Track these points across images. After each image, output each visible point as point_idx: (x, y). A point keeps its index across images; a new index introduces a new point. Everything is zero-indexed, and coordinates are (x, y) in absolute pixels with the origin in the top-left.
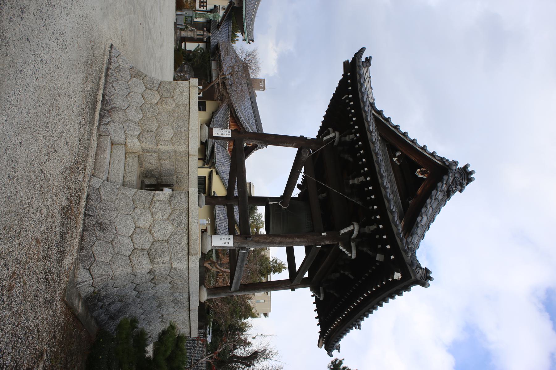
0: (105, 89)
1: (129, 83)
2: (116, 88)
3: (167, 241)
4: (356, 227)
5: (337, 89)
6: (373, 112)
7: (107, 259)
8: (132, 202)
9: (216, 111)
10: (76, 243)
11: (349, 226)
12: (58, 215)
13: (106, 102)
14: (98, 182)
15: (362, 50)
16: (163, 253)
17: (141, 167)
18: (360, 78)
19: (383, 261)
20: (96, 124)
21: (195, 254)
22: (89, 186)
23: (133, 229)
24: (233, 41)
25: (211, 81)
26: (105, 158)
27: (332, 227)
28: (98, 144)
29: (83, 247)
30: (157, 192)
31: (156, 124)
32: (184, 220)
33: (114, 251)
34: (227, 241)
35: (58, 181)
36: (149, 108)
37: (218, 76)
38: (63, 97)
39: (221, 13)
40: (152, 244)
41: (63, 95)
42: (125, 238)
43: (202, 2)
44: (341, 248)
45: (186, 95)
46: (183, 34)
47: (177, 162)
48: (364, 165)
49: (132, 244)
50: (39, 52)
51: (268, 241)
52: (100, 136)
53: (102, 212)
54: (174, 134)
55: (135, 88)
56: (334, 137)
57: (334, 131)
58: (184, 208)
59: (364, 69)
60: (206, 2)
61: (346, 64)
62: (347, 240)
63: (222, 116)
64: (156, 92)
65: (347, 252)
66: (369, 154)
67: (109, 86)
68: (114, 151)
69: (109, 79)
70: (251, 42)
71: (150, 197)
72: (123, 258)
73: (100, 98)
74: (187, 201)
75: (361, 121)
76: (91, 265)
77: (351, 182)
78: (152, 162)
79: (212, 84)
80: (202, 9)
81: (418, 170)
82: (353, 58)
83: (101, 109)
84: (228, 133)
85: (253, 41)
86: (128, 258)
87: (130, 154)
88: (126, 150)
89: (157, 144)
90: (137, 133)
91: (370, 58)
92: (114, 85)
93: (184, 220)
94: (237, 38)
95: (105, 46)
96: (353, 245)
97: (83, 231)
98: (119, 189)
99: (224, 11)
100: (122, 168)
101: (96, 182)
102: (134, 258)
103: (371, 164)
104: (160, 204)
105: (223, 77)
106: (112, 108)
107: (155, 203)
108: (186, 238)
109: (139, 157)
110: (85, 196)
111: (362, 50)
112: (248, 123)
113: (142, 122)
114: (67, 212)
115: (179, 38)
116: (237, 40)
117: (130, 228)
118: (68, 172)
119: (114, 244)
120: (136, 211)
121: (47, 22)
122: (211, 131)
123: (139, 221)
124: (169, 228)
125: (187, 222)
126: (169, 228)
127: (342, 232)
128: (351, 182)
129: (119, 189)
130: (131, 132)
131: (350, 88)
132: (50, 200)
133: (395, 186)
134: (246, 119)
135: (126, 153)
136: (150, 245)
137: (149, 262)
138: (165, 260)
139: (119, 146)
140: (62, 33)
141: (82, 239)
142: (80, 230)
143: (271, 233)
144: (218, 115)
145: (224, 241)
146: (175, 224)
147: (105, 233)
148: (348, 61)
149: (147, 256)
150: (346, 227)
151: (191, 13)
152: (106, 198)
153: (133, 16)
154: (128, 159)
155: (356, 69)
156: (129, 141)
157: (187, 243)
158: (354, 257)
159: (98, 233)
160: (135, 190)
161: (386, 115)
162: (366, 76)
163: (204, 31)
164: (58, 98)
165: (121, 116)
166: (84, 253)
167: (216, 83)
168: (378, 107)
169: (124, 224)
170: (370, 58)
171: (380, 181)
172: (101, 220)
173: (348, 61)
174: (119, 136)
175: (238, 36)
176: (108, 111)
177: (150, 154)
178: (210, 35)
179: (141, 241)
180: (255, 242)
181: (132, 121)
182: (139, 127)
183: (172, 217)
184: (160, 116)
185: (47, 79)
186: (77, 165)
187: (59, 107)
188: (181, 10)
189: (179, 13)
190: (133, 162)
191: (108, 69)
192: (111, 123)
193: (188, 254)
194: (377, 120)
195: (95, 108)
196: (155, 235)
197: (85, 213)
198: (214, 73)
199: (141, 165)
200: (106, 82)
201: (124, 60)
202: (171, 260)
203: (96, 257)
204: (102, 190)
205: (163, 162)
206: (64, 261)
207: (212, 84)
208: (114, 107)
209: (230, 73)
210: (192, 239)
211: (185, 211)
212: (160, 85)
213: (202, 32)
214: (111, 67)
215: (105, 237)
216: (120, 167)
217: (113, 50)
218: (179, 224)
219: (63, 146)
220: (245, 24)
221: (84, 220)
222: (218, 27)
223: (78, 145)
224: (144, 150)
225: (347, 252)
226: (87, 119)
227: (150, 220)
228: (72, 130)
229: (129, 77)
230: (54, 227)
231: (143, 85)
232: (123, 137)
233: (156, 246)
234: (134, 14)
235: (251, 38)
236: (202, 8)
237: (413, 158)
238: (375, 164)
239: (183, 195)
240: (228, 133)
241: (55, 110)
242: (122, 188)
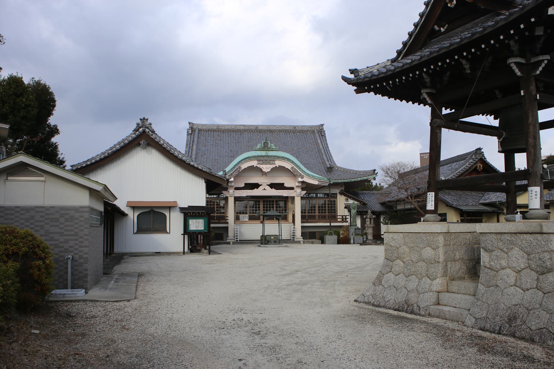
0: (390, 308)
1: (386, 286)
2: (390, 298)
3: (528, 255)
4: (511, 60)
5: (382, 96)
6: (400, 59)
7: (545, 316)
8: (491, 288)
9: (445, 203)
10: (522, 344)
11: (511, 67)
12: (483, 357)
13: (400, 308)
14: (470, 319)
15: (345, 79)
16: (540, 259)
17: (464, 278)
18: (367, 77)
19: (543, 27)
20: (418, 317)
21: (541, 227)
22: (472, 327)
23: (517, 288)
24: (382, 188)
25: (415, 209)
26: (449, 311)
27: (515, 85)
28: (437, 317)
29: (531, 338)
30: (481, 264)
31: (421, 264)
32: (507, 238)
33: (538, 308)
34: (534, 193)
35: (451, 353)
36: (408, 270)
37: (411, 203)
38: (379, 342)
39: (351, 201)
40: (532, 270)
41: (377, 342)
42: (525, 297)
43: (343, 220)
44: (538, 72)
45: (395, 236)
46: (370, 237)
47: (457, 244)
48: (497, 40)
49: (531, 290)
50: (335, 356)
51: (532, 151)
52: (430, 315)
53: (498, 317)
54: (429, 246)
55: (390, 281)
56: (427, 93)
57: (421, 94)
58: (496, 237)
59: (361, 74)
60: (342, 216)
61: (357, 92)
62: (526, 68)
63: (450, 197)
64: (394, 262)
65: (543, 65)
66: (441, 57)
67: (388, 304)
68: (445, 302)
69: (382, 304)
70: (376, 172)
71: (486, 270)
72: (545, 300)
73: (396, 313)
74: (489, 234)
75: (412, 68)
76: (551, 332)
77: (468, 71)
78: (458, 268)
79: (418, 208)
80: (349, 220)
81: (449, 5)
82: (353, 86)
83: (405, 313)
84: (431, 195)
85: (375, 170)
86: (546, 295)
87: (449, 287)
88: (444, 292)
89: (438, 262)
90: (429, 281)
91: (350, 70)
92: (387, 300)
93: (508, 237)
94: (378, 185)
95: (353, 306)
97: (514, 337)
98: (478, 300)
99: (349, 199)
100: (460, 295)
101: (470, 321)
102: (546, 289)
103: (450, 53)
104: (492, 260)
105: (409, 197)
106: (406, 303)
107: (491, 265)
108: (525, 235)
109: (453, 280)
110: (480, 332)
111: (345, 79)
112: (457, 169)
113: (419, 276)
114: (485, 349)
115: (374, 241)
116: (380, 184)
117: (516, 291)
118: (447, 345)
119: (530, 308)
120: (499, 285)
121: (315, 347)
122: (431, 212)
123: (509, 282)
124: (516, 252)
125: (509, 235)
126: (516, 252)
127: (519, 74)
128: (468, 71)
129: (478, 300)
130: (427, 286)
131: (378, 86)
132: (465, 361)
133: (468, 25)
134: (453, 172)
135: (448, 292)
136: (533, 272)
137: (551, 274)
138: (548, 257)
139: (440, 298)
140: (327, 338)
141: (522, 339)
142: (512, 339)
143: (524, 147)
144: (449, 200)
145: (534, 196)
146: (511, 246)
147: (519, 316)
148: (355, 90)
149: (544, 276)
150: (513, 71)
151: (352, 230)
152: (485, 312)
153: (337, 283)
154: (454, 291)
155: (361, 82)
156: (435, 289)
157: (530, 235)
158: (548, 57)
159: (518, 322)
160: (479, 285)
161: (400, 46)
162: (366, 71)
163: (367, 218)
164: (378, 346)
165: (413, 295)
166: (537, 339)
167: (416, 205)
168: (395, 55)
169: (511, 296)
170: (350, 70)
171: (455, 46)
172: (506, 319)
173: (355, 90)
174: (430, 298)
175: (376, 184)
176: (408, 306)
177: (449, 269)
178: (369, 211)
179: (529, 280)
180: (534, 164)
181: (418, 285)
182: (424, 279)
183: (505, 250)
184: (414, 260)
185: (358, 352)
186: (445, 336)
187: (387, 345)
188: (350, 239)
189: (352, 241)
190: (456, 285)
191: (373, 305)
192: (419, 304)
193: (542, 233)
194: (406, 55)
195: (403, 318)
196: (522, 266)
197: (497, 333)
198: (408, 206)
199: (461, 278)
200: (384, 307)
201: (367, 291)
202: (548, 251)
203: (542, 327)
204: (477, 316)
205: (458, 257)
206: (535, 357)
207: (418, 208)
208: (405, 301)
209: (406, 191)
210: (525, 230)
211: (499, 236)
212: (388, 259)
213: (367, 220)
214: (372, 302)
215: (523, 316)
216: (459, 300)
217: (359, 300)
218: (511, 242)
219: (421, 346)
220: (359, 179)
221: (504, 335)
222: (364, 204)
223: (427, 334)
224: (445, 274)
225: (543, 65)
226: (408, 324)
227: (508, 271)
228: (411, 337)
229: (381, 287)
230: (493, 361)
232: (431, 294)
233: (533, 266)
234: (337, 281)
235: (372, 172)
236: (347, 220)
237: (438, 12)
238: (440, 53)
239: (482, 238)
240: (431, 195)
241: (387, 349)
242: (477, 297)
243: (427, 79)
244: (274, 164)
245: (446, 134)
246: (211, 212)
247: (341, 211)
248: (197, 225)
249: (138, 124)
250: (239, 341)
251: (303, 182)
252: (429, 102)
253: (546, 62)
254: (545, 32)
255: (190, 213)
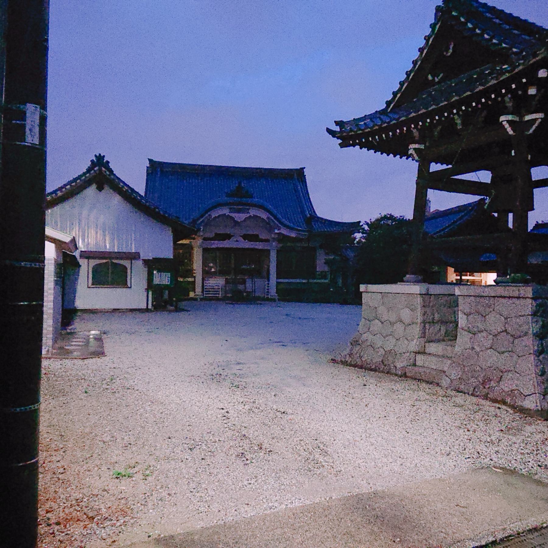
4: (502, 118)
15: (329, 131)
61: (342, 146)
64: (372, 322)
76: (522, 393)
82: (338, 139)
90: (406, 342)
91: (335, 122)
96: (527, 118)
111: (329, 131)
127: (511, 132)
131: (364, 140)
170: (335, 122)
211: (478, 299)
225: (536, 125)
231: (366, 334)
243: (416, 133)
244: (248, 213)
245: (432, 194)
246: (178, 265)
247: (321, 266)
248: (162, 279)
249: (92, 161)
250: (35, 468)
251: (279, 234)
252: (417, 158)
253: (540, 120)
254: (538, 91)
255: (152, 265)
